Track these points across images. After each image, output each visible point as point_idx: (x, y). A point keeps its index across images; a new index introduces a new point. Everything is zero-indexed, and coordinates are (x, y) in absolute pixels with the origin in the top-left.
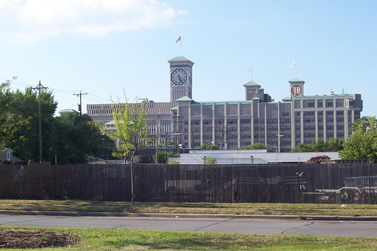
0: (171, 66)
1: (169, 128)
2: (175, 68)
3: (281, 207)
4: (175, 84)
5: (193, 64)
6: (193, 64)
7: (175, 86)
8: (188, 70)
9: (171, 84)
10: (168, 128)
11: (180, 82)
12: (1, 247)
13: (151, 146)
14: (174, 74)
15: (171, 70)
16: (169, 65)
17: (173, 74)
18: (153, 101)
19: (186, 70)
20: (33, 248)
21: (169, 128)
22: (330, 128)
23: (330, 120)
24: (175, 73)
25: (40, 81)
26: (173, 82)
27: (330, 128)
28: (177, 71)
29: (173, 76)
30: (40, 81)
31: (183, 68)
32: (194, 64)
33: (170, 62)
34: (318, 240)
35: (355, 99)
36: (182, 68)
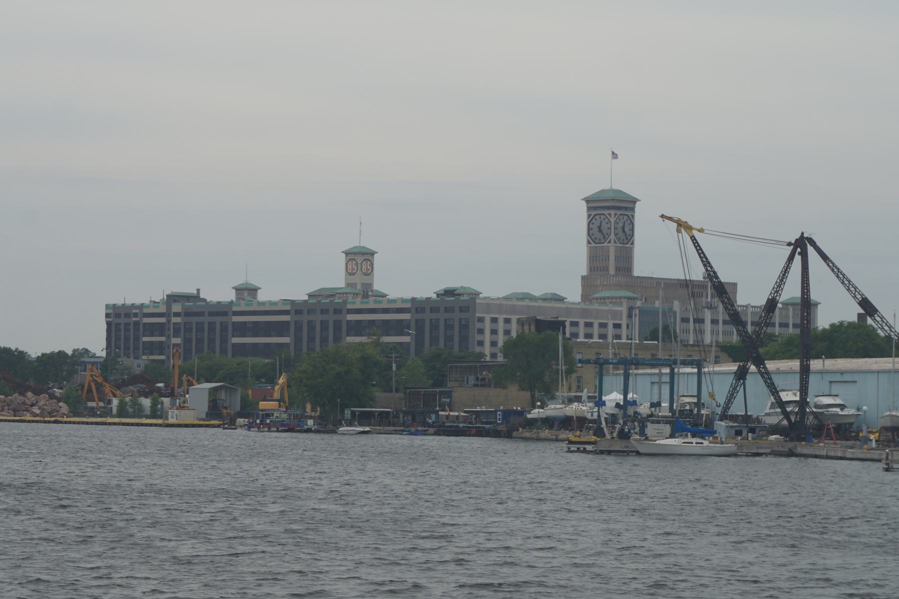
0: (589, 209)
2: (594, 213)
3: (226, 484)
5: (634, 201)
6: (634, 201)
7: (594, 245)
9: (589, 243)
11: (625, 240)
13: (668, 380)
14: (593, 224)
15: (589, 216)
16: (584, 206)
17: (591, 225)
18: (585, 273)
19: (610, 215)
22: (127, 339)
23: (127, 330)
24: (594, 221)
27: (127, 339)
28: (597, 217)
29: (590, 228)
31: (606, 212)
32: (640, 201)
33: (588, 200)
35: (791, 357)
36: (603, 212)
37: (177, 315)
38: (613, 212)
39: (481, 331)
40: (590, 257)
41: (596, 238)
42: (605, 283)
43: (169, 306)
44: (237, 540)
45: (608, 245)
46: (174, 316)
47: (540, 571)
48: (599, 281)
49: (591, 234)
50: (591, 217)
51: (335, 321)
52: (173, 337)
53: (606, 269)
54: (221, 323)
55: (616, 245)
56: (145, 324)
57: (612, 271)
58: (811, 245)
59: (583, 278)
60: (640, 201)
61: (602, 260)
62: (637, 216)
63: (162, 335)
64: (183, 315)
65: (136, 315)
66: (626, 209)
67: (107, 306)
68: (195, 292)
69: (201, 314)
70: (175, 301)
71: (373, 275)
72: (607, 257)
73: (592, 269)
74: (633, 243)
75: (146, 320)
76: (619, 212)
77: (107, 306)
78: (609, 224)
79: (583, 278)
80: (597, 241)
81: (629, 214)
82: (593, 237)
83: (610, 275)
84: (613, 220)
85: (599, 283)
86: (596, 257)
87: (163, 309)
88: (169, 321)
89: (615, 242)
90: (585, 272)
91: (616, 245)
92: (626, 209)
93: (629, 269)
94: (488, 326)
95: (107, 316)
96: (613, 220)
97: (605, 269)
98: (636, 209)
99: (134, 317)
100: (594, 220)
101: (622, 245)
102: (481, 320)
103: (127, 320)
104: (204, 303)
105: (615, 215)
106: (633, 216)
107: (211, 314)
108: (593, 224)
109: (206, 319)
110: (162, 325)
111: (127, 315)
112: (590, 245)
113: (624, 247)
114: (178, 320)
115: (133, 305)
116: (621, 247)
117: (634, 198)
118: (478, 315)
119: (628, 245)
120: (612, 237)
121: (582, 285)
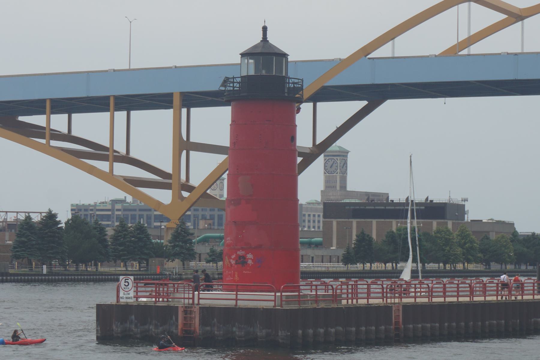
1: (218, 283)
2: (328, 158)
4: (328, 173)
5: (347, 152)
6: (347, 152)
7: (328, 174)
8: (339, 160)
9: (325, 173)
10: (154, 279)
12: (2, 281)
14: (327, 164)
15: (325, 159)
17: (326, 164)
18: (323, 189)
19: (337, 159)
20: (162, 347)
21: (218, 283)
25: (265, 29)
26: (327, 161)
28: (330, 160)
29: (326, 166)
30: (265, 29)
31: (335, 158)
34: (297, 302)
37: (118, 210)
38: (339, 158)
39: (304, 221)
40: (325, 181)
41: (329, 171)
42: (335, 194)
43: (113, 206)
44: (32, 328)
45: (336, 175)
46: (116, 211)
47: (88, 346)
48: (331, 193)
49: (326, 169)
50: (326, 160)
51: (202, 215)
52: (116, 222)
53: (335, 187)
54: (147, 215)
55: (340, 175)
56: (97, 215)
57: (338, 188)
58: (326, 170)
59: (322, 191)
60: (350, 152)
61: (333, 182)
62: (348, 159)
63: (109, 221)
64: (122, 210)
65: (92, 210)
66: (343, 156)
67: (72, 205)
68: (124, 198)
69: (135, 210)
70: (117, 203)
71: (224, 190)
72: (336, 181)
73: (327, 187)
74: (347, 174)
75: (98, 213)
76: (342, 158)
77: (72, 205)
78: (337, 164)
79: (322, 191)
80: (330, 172)
81: (345, 158)
82: (327, 171)
83: (338, 190)
84: (339, 162)
85: (331, 194)
86: (329, 181)
87: (109, 207)
88: (113, 214)
89: (340, 174)
90: (323, 188)
91: (340, 175)
92: (343, 156)
93: (345, 187)
94: (307, 218)
95: (72, 210)
96: (339, 162)
97: (334, 187)
98: (348, 156)
99: (91, 211)
100: (328, 162)
101: (342, 175)
102: (304, 215)
103: (86, 213)
104: (128, 205)
105: (340, 159)
106: (347, 160)
107: (140, 210)
108: (327, 164)
109: (137, 213)
110: (109, 216)
111: (86, 210)
112: (326, 175)
113: (343, 176)
114: (119, 213)
115: (89, 204)
116: (342, 176)
117: (348, 151)
118: (303, 213)
119: (345, 175)
120: (338, 170)
121: (321, 195)
